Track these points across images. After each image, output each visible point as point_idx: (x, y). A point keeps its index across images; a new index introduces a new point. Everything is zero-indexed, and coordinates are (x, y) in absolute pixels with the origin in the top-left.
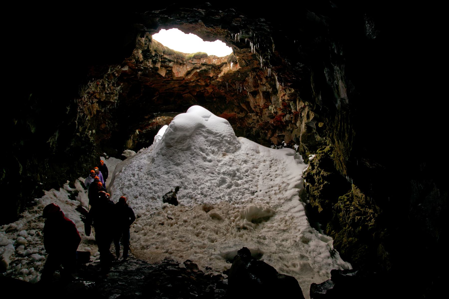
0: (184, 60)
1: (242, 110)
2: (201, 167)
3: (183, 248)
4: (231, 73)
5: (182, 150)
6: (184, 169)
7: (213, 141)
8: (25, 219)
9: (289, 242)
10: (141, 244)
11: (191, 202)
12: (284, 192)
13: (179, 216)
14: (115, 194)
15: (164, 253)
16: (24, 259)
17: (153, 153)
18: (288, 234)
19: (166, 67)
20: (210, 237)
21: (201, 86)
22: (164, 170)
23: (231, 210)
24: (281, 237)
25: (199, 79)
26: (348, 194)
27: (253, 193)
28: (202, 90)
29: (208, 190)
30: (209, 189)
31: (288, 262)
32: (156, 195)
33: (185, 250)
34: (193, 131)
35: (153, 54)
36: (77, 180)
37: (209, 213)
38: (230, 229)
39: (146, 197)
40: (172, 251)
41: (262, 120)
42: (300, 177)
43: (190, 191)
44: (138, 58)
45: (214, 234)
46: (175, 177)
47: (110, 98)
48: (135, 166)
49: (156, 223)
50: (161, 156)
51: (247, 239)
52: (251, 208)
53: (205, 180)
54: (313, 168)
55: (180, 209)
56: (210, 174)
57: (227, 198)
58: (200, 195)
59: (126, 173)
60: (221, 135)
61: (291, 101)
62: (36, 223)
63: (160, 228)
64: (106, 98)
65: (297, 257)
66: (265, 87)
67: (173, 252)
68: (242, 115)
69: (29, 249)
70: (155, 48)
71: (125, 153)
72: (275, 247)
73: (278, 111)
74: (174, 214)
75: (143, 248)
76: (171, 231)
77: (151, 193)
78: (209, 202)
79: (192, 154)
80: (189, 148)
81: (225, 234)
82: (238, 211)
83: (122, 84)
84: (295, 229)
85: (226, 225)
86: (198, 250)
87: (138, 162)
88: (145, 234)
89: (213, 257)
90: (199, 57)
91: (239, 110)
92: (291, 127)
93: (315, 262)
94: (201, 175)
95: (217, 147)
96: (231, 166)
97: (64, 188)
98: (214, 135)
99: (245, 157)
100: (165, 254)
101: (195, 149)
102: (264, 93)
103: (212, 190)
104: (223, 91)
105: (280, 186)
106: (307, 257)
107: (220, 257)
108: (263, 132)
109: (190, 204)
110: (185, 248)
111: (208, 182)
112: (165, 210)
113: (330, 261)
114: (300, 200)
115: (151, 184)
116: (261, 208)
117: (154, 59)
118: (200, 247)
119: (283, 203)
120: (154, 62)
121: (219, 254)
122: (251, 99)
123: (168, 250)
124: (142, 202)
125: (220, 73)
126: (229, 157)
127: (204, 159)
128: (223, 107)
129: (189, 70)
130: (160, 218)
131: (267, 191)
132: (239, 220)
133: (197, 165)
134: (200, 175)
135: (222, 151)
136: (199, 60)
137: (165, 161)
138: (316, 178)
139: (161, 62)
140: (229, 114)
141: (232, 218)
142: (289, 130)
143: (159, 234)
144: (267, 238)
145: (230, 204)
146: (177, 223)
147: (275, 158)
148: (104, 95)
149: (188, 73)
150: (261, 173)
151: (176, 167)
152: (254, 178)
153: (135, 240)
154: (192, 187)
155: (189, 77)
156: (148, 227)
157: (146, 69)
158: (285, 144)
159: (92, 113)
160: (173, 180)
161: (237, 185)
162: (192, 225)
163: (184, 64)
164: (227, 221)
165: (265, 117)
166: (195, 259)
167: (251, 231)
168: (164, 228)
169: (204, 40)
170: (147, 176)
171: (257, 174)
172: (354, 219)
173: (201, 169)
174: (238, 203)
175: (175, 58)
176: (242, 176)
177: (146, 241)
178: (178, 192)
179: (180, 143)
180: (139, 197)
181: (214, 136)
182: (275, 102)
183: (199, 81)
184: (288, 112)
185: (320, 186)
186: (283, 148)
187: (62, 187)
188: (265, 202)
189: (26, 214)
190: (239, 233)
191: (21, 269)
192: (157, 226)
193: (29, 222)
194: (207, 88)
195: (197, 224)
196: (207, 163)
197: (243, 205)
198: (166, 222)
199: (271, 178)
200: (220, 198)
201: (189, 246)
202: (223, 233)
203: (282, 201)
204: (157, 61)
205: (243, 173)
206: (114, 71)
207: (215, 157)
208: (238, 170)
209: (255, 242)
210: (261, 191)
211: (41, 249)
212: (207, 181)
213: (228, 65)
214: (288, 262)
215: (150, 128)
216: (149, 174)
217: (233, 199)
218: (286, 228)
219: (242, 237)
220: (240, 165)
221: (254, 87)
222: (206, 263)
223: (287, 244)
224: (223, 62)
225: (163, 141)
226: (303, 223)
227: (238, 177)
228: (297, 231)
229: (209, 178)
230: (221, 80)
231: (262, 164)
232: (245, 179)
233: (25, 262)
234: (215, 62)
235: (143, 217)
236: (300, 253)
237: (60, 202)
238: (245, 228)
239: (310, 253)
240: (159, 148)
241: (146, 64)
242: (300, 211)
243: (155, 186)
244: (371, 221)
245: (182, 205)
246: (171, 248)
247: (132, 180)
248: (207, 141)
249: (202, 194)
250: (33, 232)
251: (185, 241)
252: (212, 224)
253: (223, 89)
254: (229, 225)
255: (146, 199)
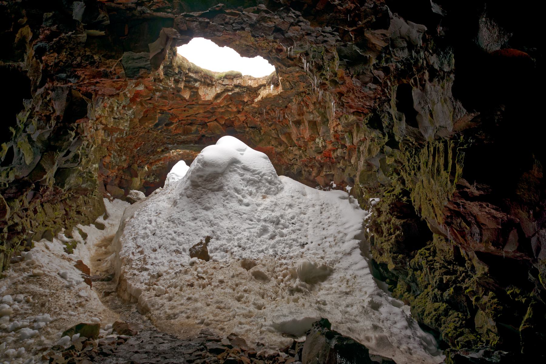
0: (214, 80)
1: (281, 143)
2: (236, 212)
3: (223, 317)
4: (270, 98)
5: (213, 191)
6: (215, 214)
7: (250, 180)
8: (9, 280)
9: (355, 307)
10: (166, 312)
11: (226, 256)
12: (341, 244)
13: (212, 274)
14: (126, 247)
15: (199, 324)
16: (10, 336)
17: (174, 193)
18: (352, 298)
19: (191, 88)
20: (256, 302)
21: (231, 113)
22: (190, 215)
23: (277, 266)
24: (344, 302)
25: (230, 104)
26: (428, 247)
27: (303, 245)
28: (233, 118)
29: (246, 241)
30: (248, 239)
31: (359, 334)
32: (181, 247)
33: (226, 320)
34: (226, 166)
35: (177, 71)
36: (74, 228)
37: (251, 270)
38: (280, 291)
39: (168, 250)
40: (209, 322)
41: (306, 156)
42: (360, 225)
43: (224, 242)
44: (159, 75)
45: (260, 298)
46: (205, 224)
47: (119, 124)
48: (151, 210)
49: (183, 284)
50: (186, 197)
51: (304, 305)
52: (304, 265)
53: (242, 229)
54: (379, 216)
55: (213, 266)
56: (248, 221)
57: (271, 252)
58: (238, 247)
59: (139, 218)
60: (260, 172)
61: (346, 132)
62: (24, 285)
63: (189, 291)
64: (114, 124)
65: (369, 328)
66: (312, 116)
67: (211, 324)
68: (280, 149)
69: (16, 322)
70: (179, 63)
71: (131, 194)
72: (340, 315)
73: (327, 145)
74: (206, 272)
75: (169, 317)
76: (204, 294)
77: (174, 245)
78: (249, 257)
79: (225, 196)
80: (220, 189)
81: (274, 299)
82: (287, 269)
83: (134, 107)
84: (360, 290)
85: (273, 287)
86: (243, 320)
87: (155, 205)
88: (170, 299)
89: (263, 329)
90: (232, 77)
91: (277, 143)
92: (343, 164)
93: (392, 334)
94: (236, 222)
95: (256, 187)
96: (273, 211)
97: (59, 238)
98: (251, 172)
99: (289, 201)
100: (199, 326)
101: (228, 189)
102: (310, 122)
103: (252, 241)
104: (259, 120)
105: (336, 237)
106: (382, 328)
107: (272, 329)
108: (307, 170)
109: (224, 260)
110: (225, 318)
111: (245, 231)
112: (194, 267)
113: (409, 332)
114: (361, 254)
115: (173, 233)
116: (316, 265)
117: (177, 78)
118: (245, 316)
119: (341, 258)
120: (177, 82)
121: (271, 326)
122: (294, 130)
123: (204, 320)
124: (162, 257)
125: (257, 97)
126: (270, 199)
127: (240, 202)
128: (258, 138)
129: (219, 92)
130: (188, 277)
131: (320, 242)
132: (289, 280)
133: (231, 210)
134: (235, 223)
135: (261, 193)
136: (231, 81)
137: (191, 205)
138: (384, 228)
139: (185, 81)
140: (264, 147)
141: (280, 278)
142: (340, 168)
143: (189, 299)
144: (327, 302)
145: (276, 259)
146: (210, 284)
147: (326, 202)
148: (112, 120)
149: (218, 96)
150: (311, 221)
151: (205, 212)
152: (302, 226)
153: (156, 307)
154: (227, 237)
155: (219, 101)
156: (173, 289)
157: (165, 89)
158: (334, 185)
159: (96, 141)
160: (202, 228)
161: (282, 235)
162: (230, 287)
163: (213, 85)
164: (274, 282)
165: (311, 153)
166: (240, 332)
167: (306, 294)
168: (195, 290)
169: (242, 56)
170: (167, 223)
171: (306, 221)
172: (441, 280)
173: (236, 215)
174: (285, 258)
175: (202, 77)
176: (288, 224)
177: (173, 307)
178: (209, 243)
179: (207, 183)
180: (159, 250)
181: (251, 174)
182: (324, 133)
183: (230, 106)
184: (340, 146)
185: (391, 237)
186: (331, 190)
187: (56, 236)
188: (319, 256)
189: (10, 272)
190: (292, 297)
191: (6, 349)
192: (185, 288)
193: (15, 284)
194: (239, 115)
195: (237, 285)
196: (244, 207)
197: (292, 260)
198: (196, 283)
199: (324, 226)
200: (262, 251)
201: (231, 314)
202: (271, 296)
203: (340, 256)
204: (181, 80)
205: (288, 220)
206: (127, 90)
207: (254, 200)
208: (282, 216)
209: (315, 309)
210: (312, 243)
211: (32, 320)
212: (244, 230)
213: (267, 87)
214: (359, 334)
215: (162, 164)
216: (171, 220)
217: (279, 253)
218: (348, 290)
219: (297, 302)
220: (284, 210)
221: (299, 115)
222: (256, 337)
223: (353, 310)
224: (260, 83)
225: (188, 179)
226: (368, 283)
227: (282, 225)
228: (363, 293)
229: (247, 226)
230: (257, 106)
231: (311, 209)
232: (291, 228)
233: (11, 339)
234: (251, 83)
235: (165, 276)
236: (372, 323)
237: (54, 256)
238: (298, 290)
239: (383, 322)
240: (183, 188)
241: (167, 83)
242: (363, 268)
243: (179, 235)
244: (464, 282)
245: (215, 261)
246: (208, 318)
247: (149, 228)
248: (243, 180)
249: (240, 247)
250: (21, 297)
251: (224, 308)
252: (256, 286)
253: (258, 117)
254: (277, 286)
255: (168, 252)
